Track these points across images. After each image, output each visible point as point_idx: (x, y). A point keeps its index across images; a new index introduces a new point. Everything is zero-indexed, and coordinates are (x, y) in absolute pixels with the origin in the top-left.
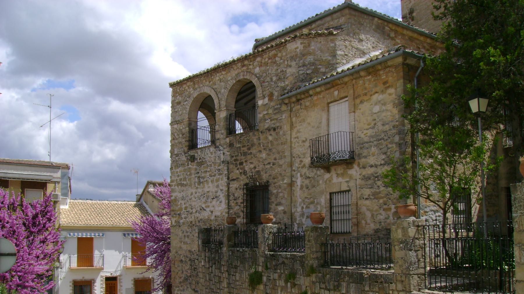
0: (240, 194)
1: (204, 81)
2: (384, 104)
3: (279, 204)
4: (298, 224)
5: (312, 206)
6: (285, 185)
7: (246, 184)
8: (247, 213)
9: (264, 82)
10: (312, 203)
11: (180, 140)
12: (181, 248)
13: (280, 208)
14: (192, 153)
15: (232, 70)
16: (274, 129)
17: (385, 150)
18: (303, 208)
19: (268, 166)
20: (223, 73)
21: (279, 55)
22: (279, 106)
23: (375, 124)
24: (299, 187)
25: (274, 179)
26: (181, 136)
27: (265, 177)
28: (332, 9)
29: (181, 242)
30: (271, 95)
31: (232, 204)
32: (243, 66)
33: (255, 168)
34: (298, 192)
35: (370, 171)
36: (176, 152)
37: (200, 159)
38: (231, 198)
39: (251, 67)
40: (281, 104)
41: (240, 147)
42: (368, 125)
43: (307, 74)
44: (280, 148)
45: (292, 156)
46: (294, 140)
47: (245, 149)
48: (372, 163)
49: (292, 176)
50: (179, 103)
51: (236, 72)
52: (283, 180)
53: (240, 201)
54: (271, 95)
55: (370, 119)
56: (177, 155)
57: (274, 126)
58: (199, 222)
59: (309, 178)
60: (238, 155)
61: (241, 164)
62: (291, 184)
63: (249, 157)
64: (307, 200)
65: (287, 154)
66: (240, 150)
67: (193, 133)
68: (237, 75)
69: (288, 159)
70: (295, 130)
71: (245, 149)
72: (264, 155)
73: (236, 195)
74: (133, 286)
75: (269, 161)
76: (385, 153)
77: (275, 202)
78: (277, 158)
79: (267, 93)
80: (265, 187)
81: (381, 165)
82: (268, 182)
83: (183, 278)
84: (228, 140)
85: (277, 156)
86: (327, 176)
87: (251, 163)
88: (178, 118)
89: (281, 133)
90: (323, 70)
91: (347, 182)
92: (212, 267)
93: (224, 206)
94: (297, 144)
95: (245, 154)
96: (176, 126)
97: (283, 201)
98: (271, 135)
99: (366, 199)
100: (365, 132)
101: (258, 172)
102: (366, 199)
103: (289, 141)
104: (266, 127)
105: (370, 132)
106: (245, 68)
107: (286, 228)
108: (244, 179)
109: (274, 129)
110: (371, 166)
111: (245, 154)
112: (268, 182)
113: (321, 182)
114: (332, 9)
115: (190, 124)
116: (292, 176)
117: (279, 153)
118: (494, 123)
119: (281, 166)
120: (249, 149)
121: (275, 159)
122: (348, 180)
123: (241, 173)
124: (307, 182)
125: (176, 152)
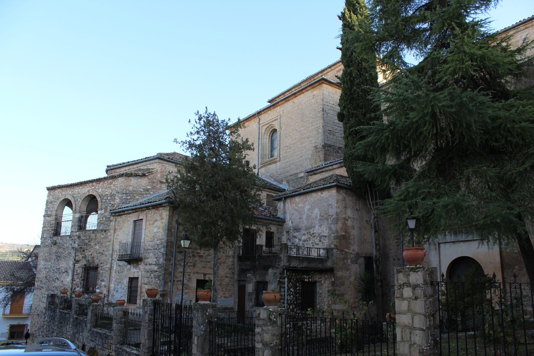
0: (80, 271)
1: (68, 191)
2: (159, 228)
3: (103, 281)
4: (112, 295)
5: (120, 284)
6: (107, 269)
7: (85, 265)
8: (84, 285)
9: (103, 199)
10: (120, 282)
11: (48, 228)
12: (39, 305)
13: (103, 283)
14: (55, 238)
15: (86, 187)
16: (105, 231)
17: (156, 256)
18: (115, 285)
19: (99, 255)
20: (81, 187)
21: (114, 183)
22: (109, 216)
23: (154, 239)
24: (115, 271)
25: (101, 263)
26: (49, 225)
27: (97, 261)
28: (499, 31)
29: (40, 301)
30: (106, 209)
31: (75, 277)
32: (93, 186)
33: (91, 255)
34: (113, 274)
35: (148, 267)
36: (45, 237)
37: (59, 243)
38: (75, 273)
39: (97, 187)
40: (110, 215)
41: (84, 240)
42: (151, 239)
43: (127, 199)
44: (108, 244)
45: (113, 251)
46: (115, 240)
47: (87, 241)
48: (151, 262)
49: (111, 263)
50: (51, 202)
51: (88, 189)
52: (107, 265)
53: (80, 276)
54: (106, 209)
55: (152, 235)
56: (45, 238)
57: (105, 229)
58: (53, 287)
59: (120, 266)
60: (82, 245)
61: (84, 251)
62: (111, 268)
63: (89, 247)
64: (117, 280)
65: (111, 248)
66: (84, 241)
67: (58, 225)
68: (89, 191)
69: (111, 252)
70: (116, 234)
71: (87, 241)
72: (97, 247)
73: (78, 272)
74: (8, 331)
75: (100, 251)
76: (156, 258)
77: (101, 279)
78: (105, 250)
79: (103, 206)
80: (96, 268)
81: (154, 264)
82: (98, 265)
83: (37, 328)
84: (78, 233)
85: (105, 249)
86: (129, 266)
87: (90, 251)
88: (49, 213)
89: (109, 234)
90: (137, 197)
91: (138, 272)
92: (50, 321)
93: (69, 279)
94: (116, 243)
95: (86, 244)
96: (47, 218)
97: (105, 279)
98: (103, 234)
99: (146, 284)
100: (149, 243)
101: (93, 258)
102: (146, 284)
103: (112, 240)
104: (101, 229)
105: (151, 244)
106: (93, 187)
107: (105, 297)
108: (83, 262)
109: (105, 231)
110: (150, 264)
111: (86, 244)
112: (98, 265)
113: (125, 270)
114: (499, 31)
115: (56, 219)
116: (111, 263)
117: (106, 247)
118: (349, 226)
119: (106, 255)
120: (89, 242)
121: (104, 251)
122: (138, 271)
123: (83, 257)
124: (119, 268)
125: (45, 237)
